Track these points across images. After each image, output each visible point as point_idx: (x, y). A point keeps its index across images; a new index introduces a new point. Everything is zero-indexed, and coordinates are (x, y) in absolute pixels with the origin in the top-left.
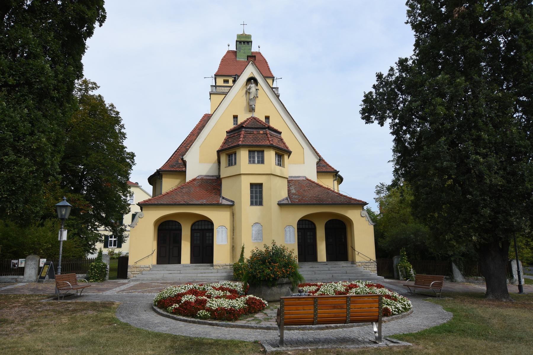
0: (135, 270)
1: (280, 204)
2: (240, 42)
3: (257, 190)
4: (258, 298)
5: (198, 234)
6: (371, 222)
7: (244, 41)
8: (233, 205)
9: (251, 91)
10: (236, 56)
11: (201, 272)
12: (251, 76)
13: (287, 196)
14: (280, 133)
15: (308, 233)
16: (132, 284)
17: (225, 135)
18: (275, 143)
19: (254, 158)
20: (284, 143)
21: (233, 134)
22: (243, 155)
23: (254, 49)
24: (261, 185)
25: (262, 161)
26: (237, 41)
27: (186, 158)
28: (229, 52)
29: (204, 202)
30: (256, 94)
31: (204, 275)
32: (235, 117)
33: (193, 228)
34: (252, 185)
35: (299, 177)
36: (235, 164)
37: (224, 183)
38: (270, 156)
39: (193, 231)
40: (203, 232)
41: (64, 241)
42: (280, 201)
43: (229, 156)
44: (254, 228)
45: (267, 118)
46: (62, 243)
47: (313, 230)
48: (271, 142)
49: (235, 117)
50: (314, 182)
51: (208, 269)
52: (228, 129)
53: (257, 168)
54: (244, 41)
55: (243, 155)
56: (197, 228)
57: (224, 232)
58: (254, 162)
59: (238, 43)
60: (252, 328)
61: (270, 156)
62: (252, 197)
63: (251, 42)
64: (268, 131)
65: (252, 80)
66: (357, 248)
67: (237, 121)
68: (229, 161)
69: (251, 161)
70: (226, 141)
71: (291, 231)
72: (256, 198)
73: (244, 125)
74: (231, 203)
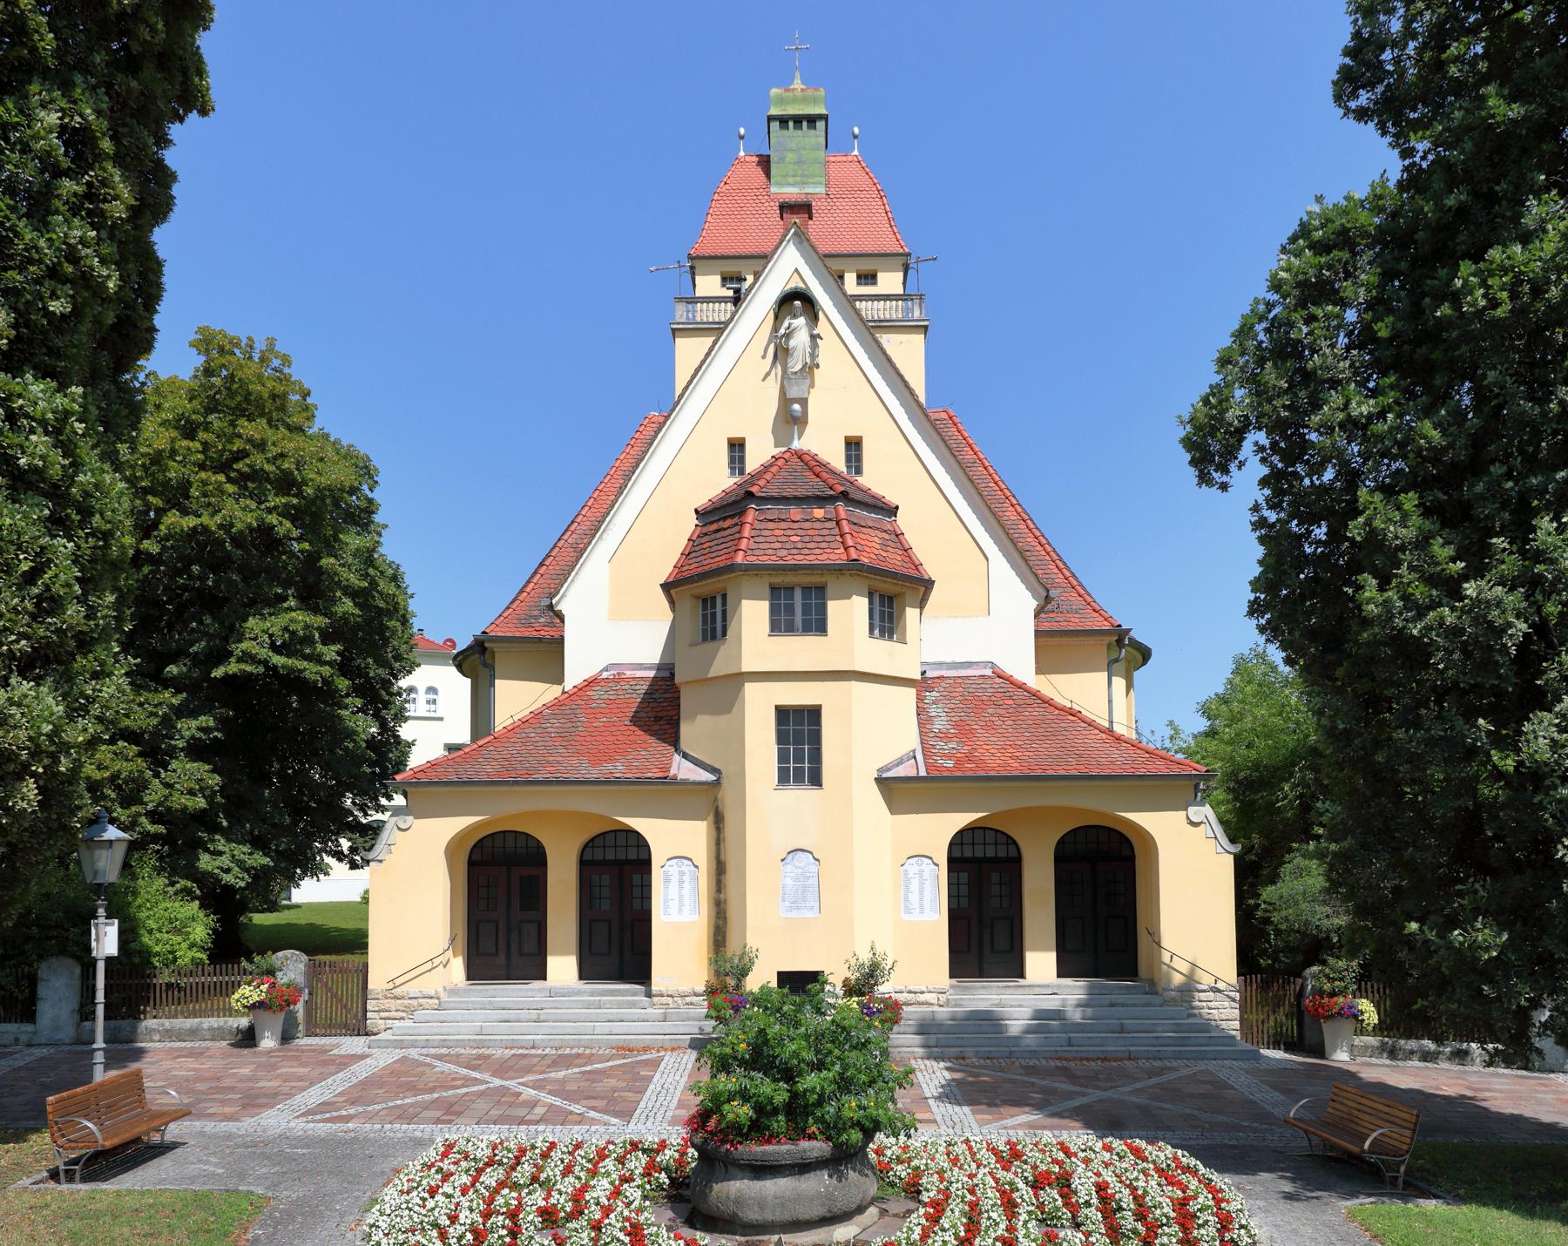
0: (392, 1004)
1: (886, 785)
3: (800, 733)
6: (1224, 841)
8: (717, 784)
9: (792, 343)
10: (768, 174)
11: (612, 1013)
12: (792, 285)
14: (892, 511)
15: (995, 877)
16: (381, 1059)
17: (690, 523)
18: (870, 548)
19: (790, 609)
20: (907, 550)
21: (720, 516)
22: (753, 614)
24: (814, 713)
25: (817, 624)
27: (564, 607)
29: (618, 769)
30: (813, 355)
31: (617, 1027)
32: (737, 447)
33: (588, 857)
34: (783, 713)
35: (969, 665)
36: (724, 634)
38: (849, 613)
40: (618, 874)
41: (109, 960)
44: (789, 868)
45: (854, 446)
46: (101, 966)
47: (1011, 865)
48: (854, 554)
49: (737, 447)
50: (1021, 686)
51: (633, 1005)
52: (703, 498)
53: (800, 651)
55: (753, 614)
56: (599, 856)
57: (687, 878)
58: (790, 629)
59: (775, 125)
61: (849, 613)
62: (783, 757)
64: (842, 509)
65: (795, 301)
66: (1166, 941)
67: (742, 460)
69: (781, 624)
70: (694, 548)
71: (926, 876)
72: (799, 758)
73: (754, 489)
74: (711, 777)
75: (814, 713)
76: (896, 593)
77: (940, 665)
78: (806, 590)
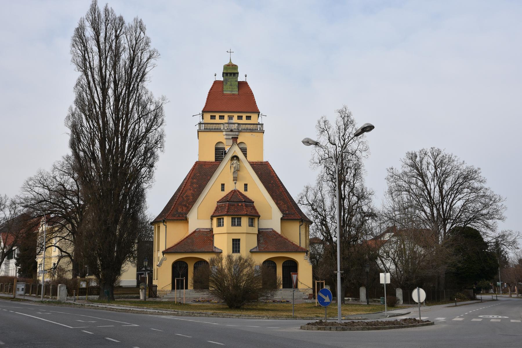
7: (231, 71)
12: (234, 155)
14: (253, 202)
17: (215, 205)
19: (235, 222)
20: (256, 210)
24: (239, 240)
25: (239, 225)
26: (223, 73)
28: (216, 82)
34: (233, 240)
38: (245, 221)
43: (219, 220)
53: (237, 229)
54: (231, 71)
55: (227, 220)
59: (225, 75)
60: (71, 304)
61: (245, 221)
63: (238, 73)
69: (233, 224)
72: (236, 248)
75: (239, 240)
76: (254, 216)
77: (204, 229)
78: (238, 218)
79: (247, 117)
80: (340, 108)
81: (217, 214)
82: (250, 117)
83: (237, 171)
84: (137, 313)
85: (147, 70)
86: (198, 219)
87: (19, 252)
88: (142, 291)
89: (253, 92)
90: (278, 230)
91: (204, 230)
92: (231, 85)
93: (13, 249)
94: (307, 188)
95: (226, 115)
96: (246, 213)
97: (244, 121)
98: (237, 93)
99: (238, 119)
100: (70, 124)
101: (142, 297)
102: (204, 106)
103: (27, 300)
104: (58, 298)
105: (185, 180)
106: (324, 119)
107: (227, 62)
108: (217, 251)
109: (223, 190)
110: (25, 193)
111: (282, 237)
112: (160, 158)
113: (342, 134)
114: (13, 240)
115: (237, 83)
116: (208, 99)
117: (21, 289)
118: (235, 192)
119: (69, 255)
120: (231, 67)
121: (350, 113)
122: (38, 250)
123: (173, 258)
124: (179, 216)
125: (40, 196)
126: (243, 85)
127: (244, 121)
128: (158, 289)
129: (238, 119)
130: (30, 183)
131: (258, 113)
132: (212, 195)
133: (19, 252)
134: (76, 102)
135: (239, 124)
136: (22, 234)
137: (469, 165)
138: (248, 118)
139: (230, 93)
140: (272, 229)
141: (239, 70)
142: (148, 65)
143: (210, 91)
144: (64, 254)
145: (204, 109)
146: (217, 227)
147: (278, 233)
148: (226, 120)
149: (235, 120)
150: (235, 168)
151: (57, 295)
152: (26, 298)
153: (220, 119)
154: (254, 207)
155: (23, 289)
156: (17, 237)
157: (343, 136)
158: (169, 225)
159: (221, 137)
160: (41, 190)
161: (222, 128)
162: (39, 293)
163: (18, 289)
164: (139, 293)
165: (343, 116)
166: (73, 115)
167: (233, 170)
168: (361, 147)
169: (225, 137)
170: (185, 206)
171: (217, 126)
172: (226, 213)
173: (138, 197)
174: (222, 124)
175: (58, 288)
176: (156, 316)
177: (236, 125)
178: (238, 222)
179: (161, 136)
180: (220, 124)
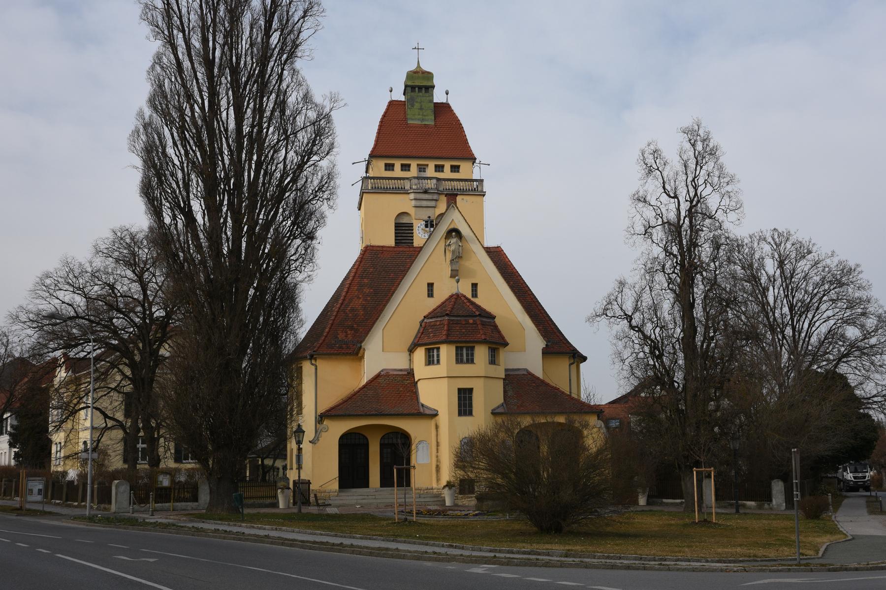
2: (413, 88)
4: (248, 474)
5: (389, 450)
7: (419, 84)
12: (452, 227)
13: (502, 401)
14: (494, 317)
19: (462, 355)
20: (499, 332)
23: (438, 97)
24: (471, 390)
25: (470, 361)
26: (406, 86)
28: (392, 104)
34: (460, 390)
35: (519, 370)
37: (421, 386)
38: (481, 353)
39: (382, 446)
42: (494, 410)
43: (429, 352)
53: (466, 369)
54: (419, 84)
55: (446, 352)
56: (386, 442)
59: (409, 89)
61: (481, 353)
68: (429, 357)
69: (459, 360)
75: (471, 390)
76: (497, 342)
77: (395, 370)
78: (467, 348)
79: (452, 167)
80: (688, 123)
81: (426, 340)
82: (458, 167)
83: (457, 258)
84: (371, 554)
85: (303, 36)
86: (382, 353)
87: (15, 423)
88: (282, 492)
89: (462, 122)
90: (538, 372)
91: (400, 373)
92: (421, 109)
93: (5, 416)
94: (622, 284)
95: (414, 164)
96: (483, 337)
97: (447, 174)
98: (433, 123)
99: (436, 171)
100: (140, 145)
101: (281, 505)
102: (372, 146)
103: (50, 513)
104: (113, 507)
105: (345, 279)
106: (652, 147)
107: (413, 67)
108: (428, 412)
109: (430, 294)
110: (38, 301)
111: (548, 385)
112: (328, 221)
113: (690, 179)
114: (4, 401)
115: (432, 105)
116: (379, 133)
117: (35, 491)
118: (457, 298)
119: (121, 425)
120: (420, 75)
121: (708, 133)
122: (54, 415)
123: (338, 428)
124: (341, 347)
125: (70, 309)
126: (443, 109)
127: (447, 174)
128: (312, 487)
129: (436, 171)
130: (48, 281)
131: (473, 160)
132: (410, 305)
133: (15, 423)
134: (152, 102)
135: (438, 180)
136: (18, 390)
137: (843, 258)
138: (455, 169)
139: (419, 123)
140: (526, 370)
141: (436, 81)
142: (306, 26)
143: (382, 119)
144: (110, 423)
145: (372, 152)
146: (426, 365)
147: (538, 378)
148: (414, 171)
149: (430, 172)
150: (453, 252)
151: (110, 502)
152: (48, 508)
153: (402, 170)
154: (496, 327)
155: (40, 490)
156: (12, 394)
157: (694, 180)
158: (321, 363)
159: (405, 203)
160: (67, 296)
161: (407, 187)
162: (84, 499)
163: (31, 491)
164: (276, 497)
165: (692, 141)
166: (146, 126)
167: (449, 256)
168: (726, 201)
169: (413, 203)
170: (352, 328)
171: (398, 184)
172: (444, 337)
173: (288, 298)
174: (407, 178)
175: (113, 488)
176: (429, 564)
177: (434, 181)
178: (467, 355)
179: (330, 176)
180: (404, 179)
